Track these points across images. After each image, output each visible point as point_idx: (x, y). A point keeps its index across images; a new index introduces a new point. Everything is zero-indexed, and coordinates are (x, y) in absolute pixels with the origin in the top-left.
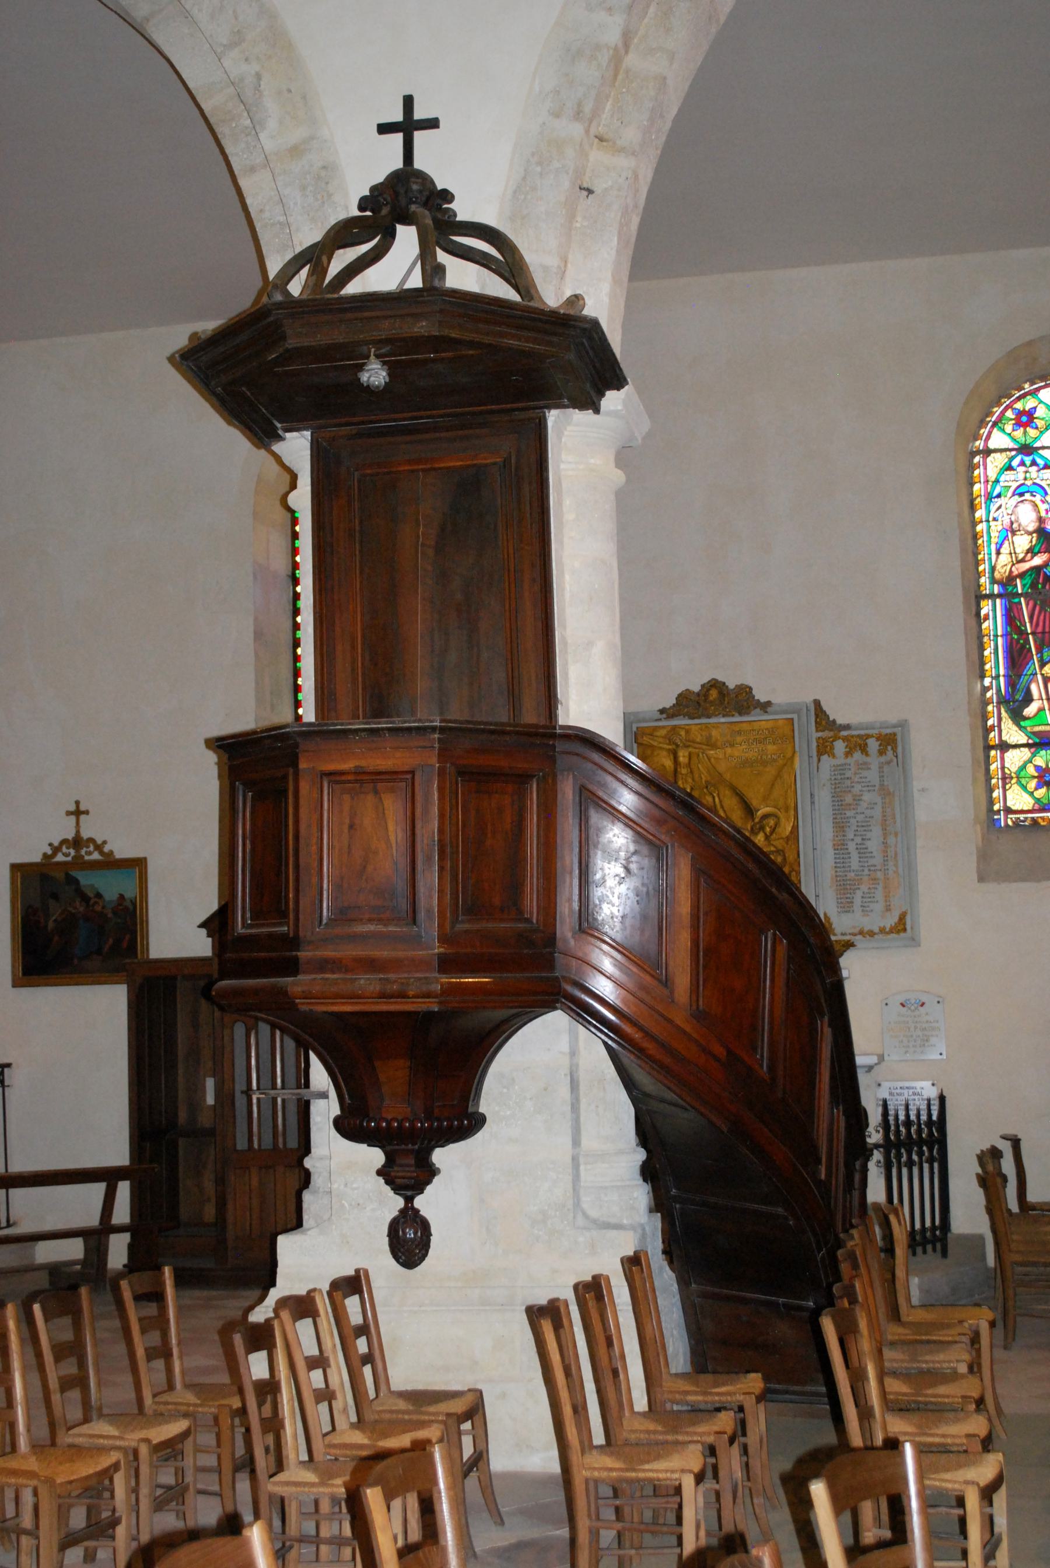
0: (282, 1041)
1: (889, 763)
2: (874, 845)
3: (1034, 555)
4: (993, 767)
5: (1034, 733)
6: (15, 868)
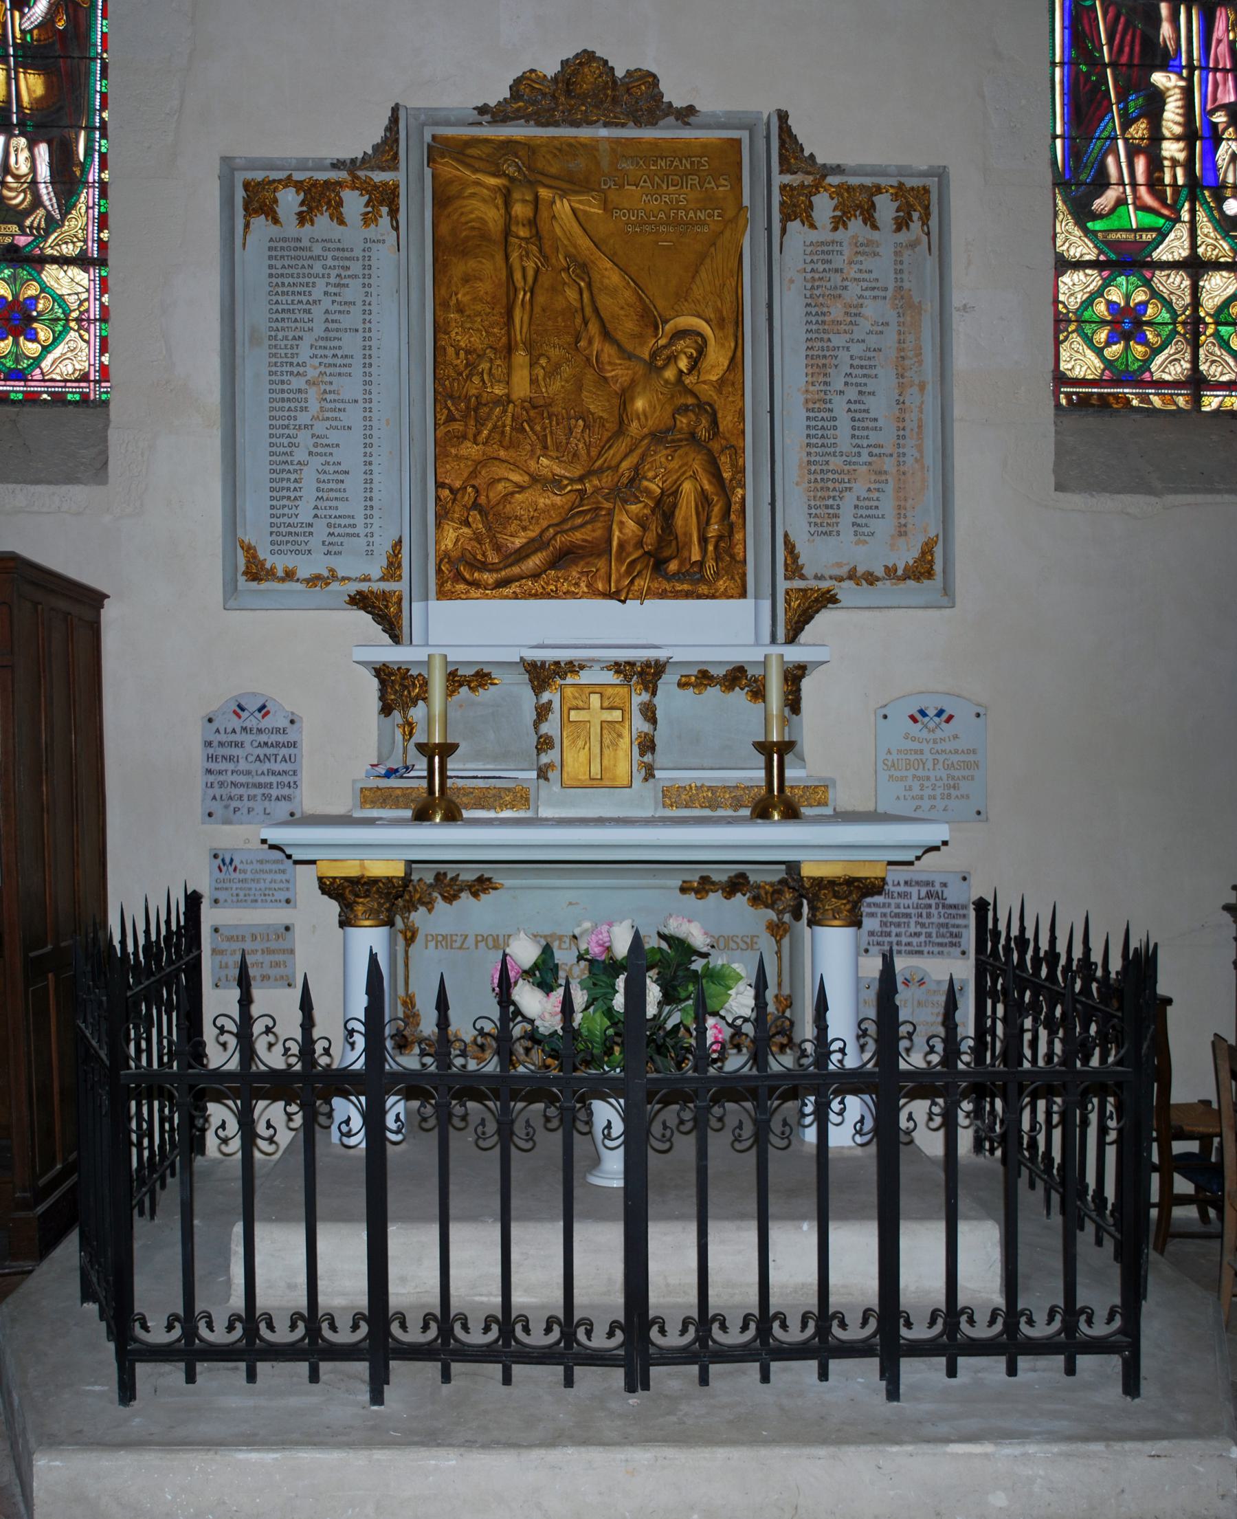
1: (913, 245)
2: (880, 406)
5: (1109, 244)
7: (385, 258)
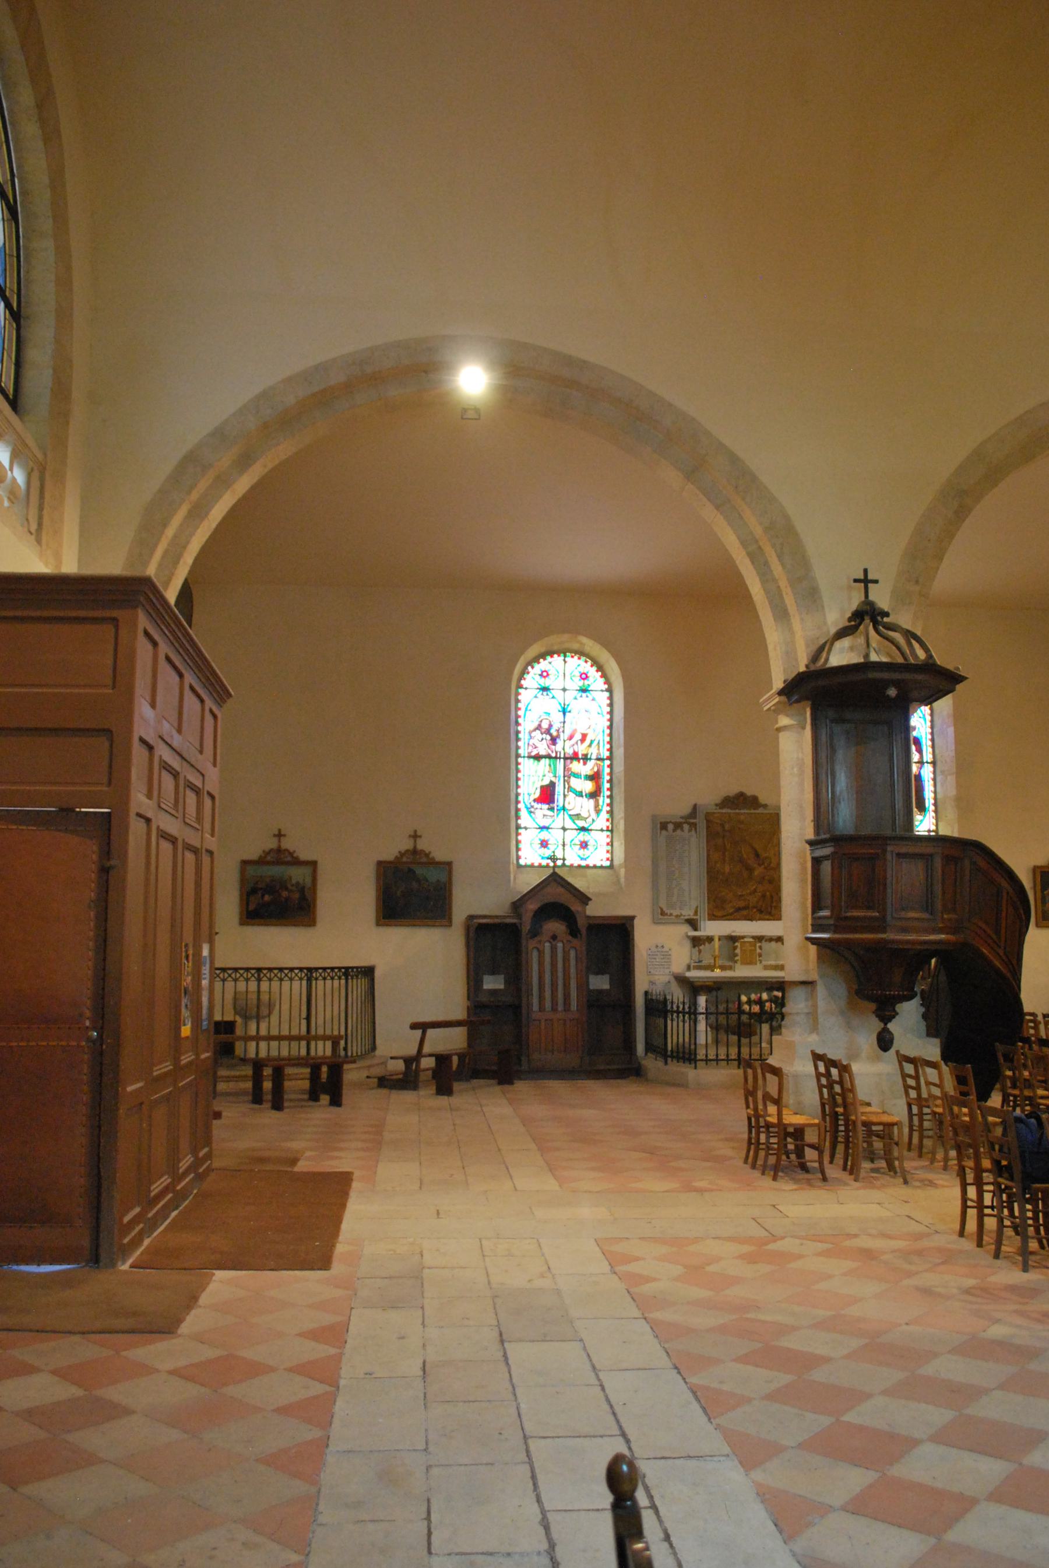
6: (380, 863)
7: (694, 840)
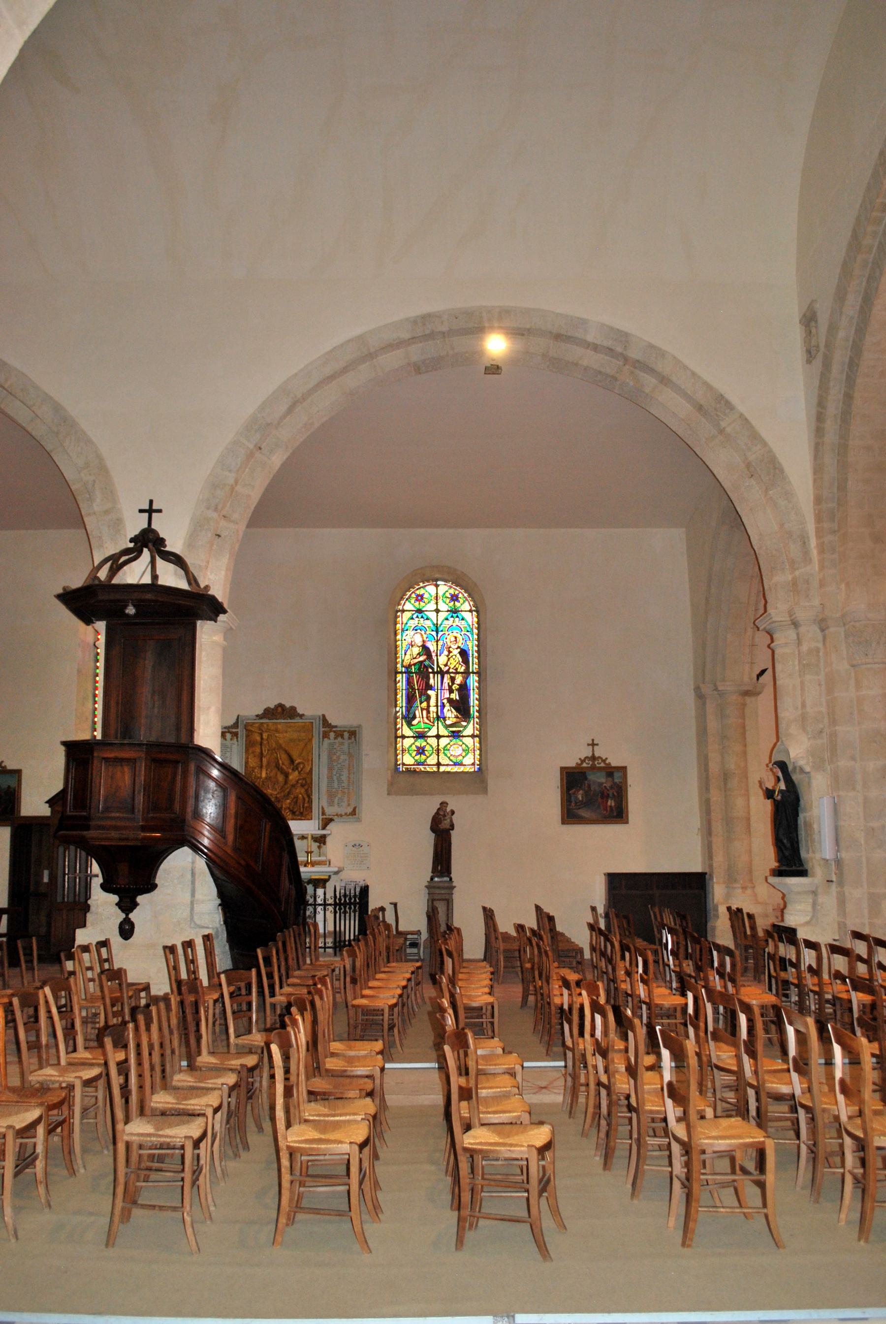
0: (80, 854)
1: (352, 743)
3: (420, 656)
4: (398, 746)
